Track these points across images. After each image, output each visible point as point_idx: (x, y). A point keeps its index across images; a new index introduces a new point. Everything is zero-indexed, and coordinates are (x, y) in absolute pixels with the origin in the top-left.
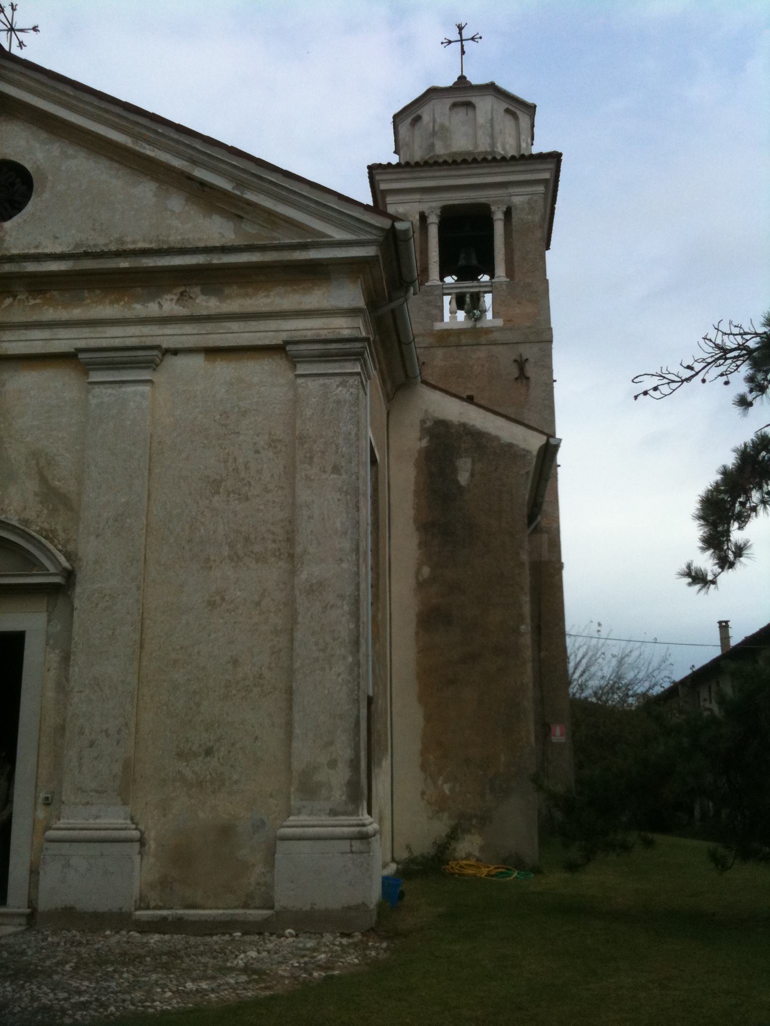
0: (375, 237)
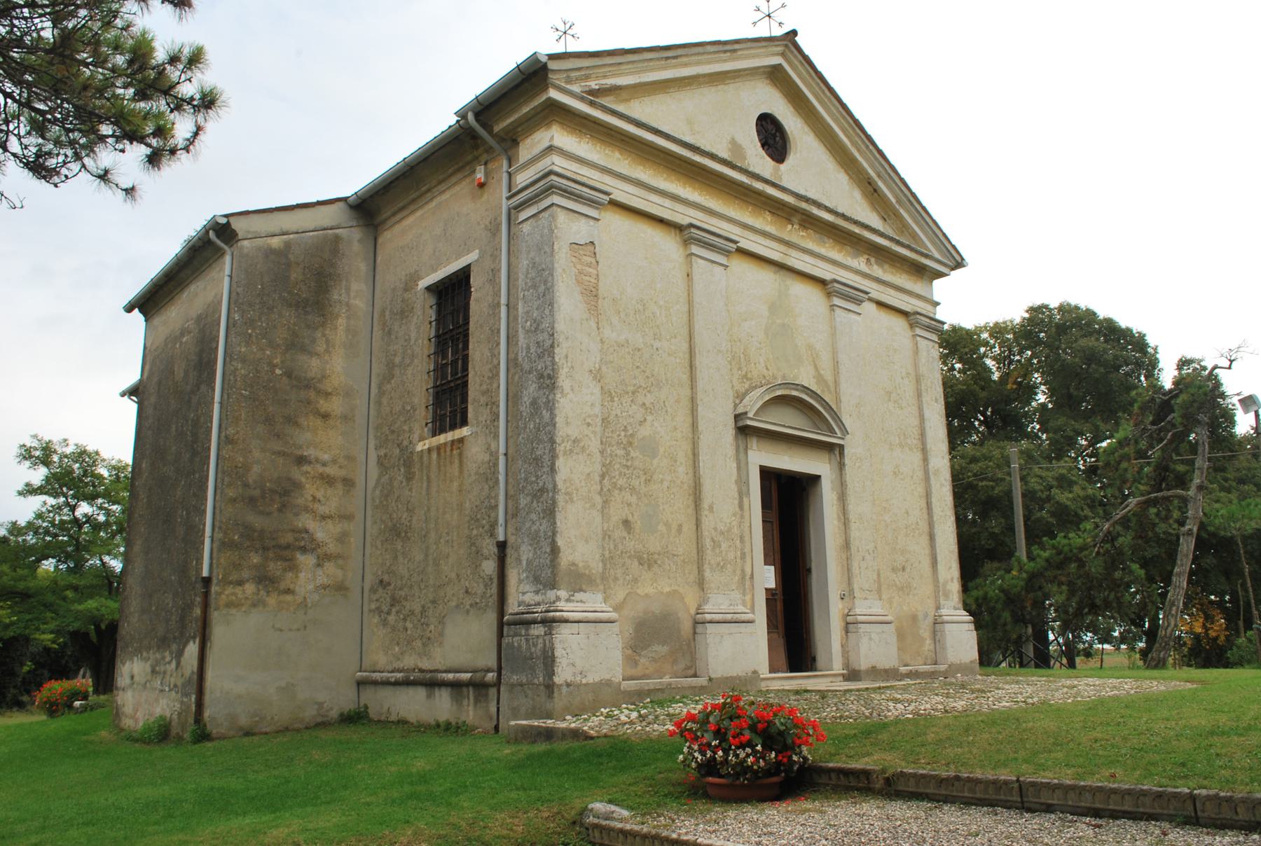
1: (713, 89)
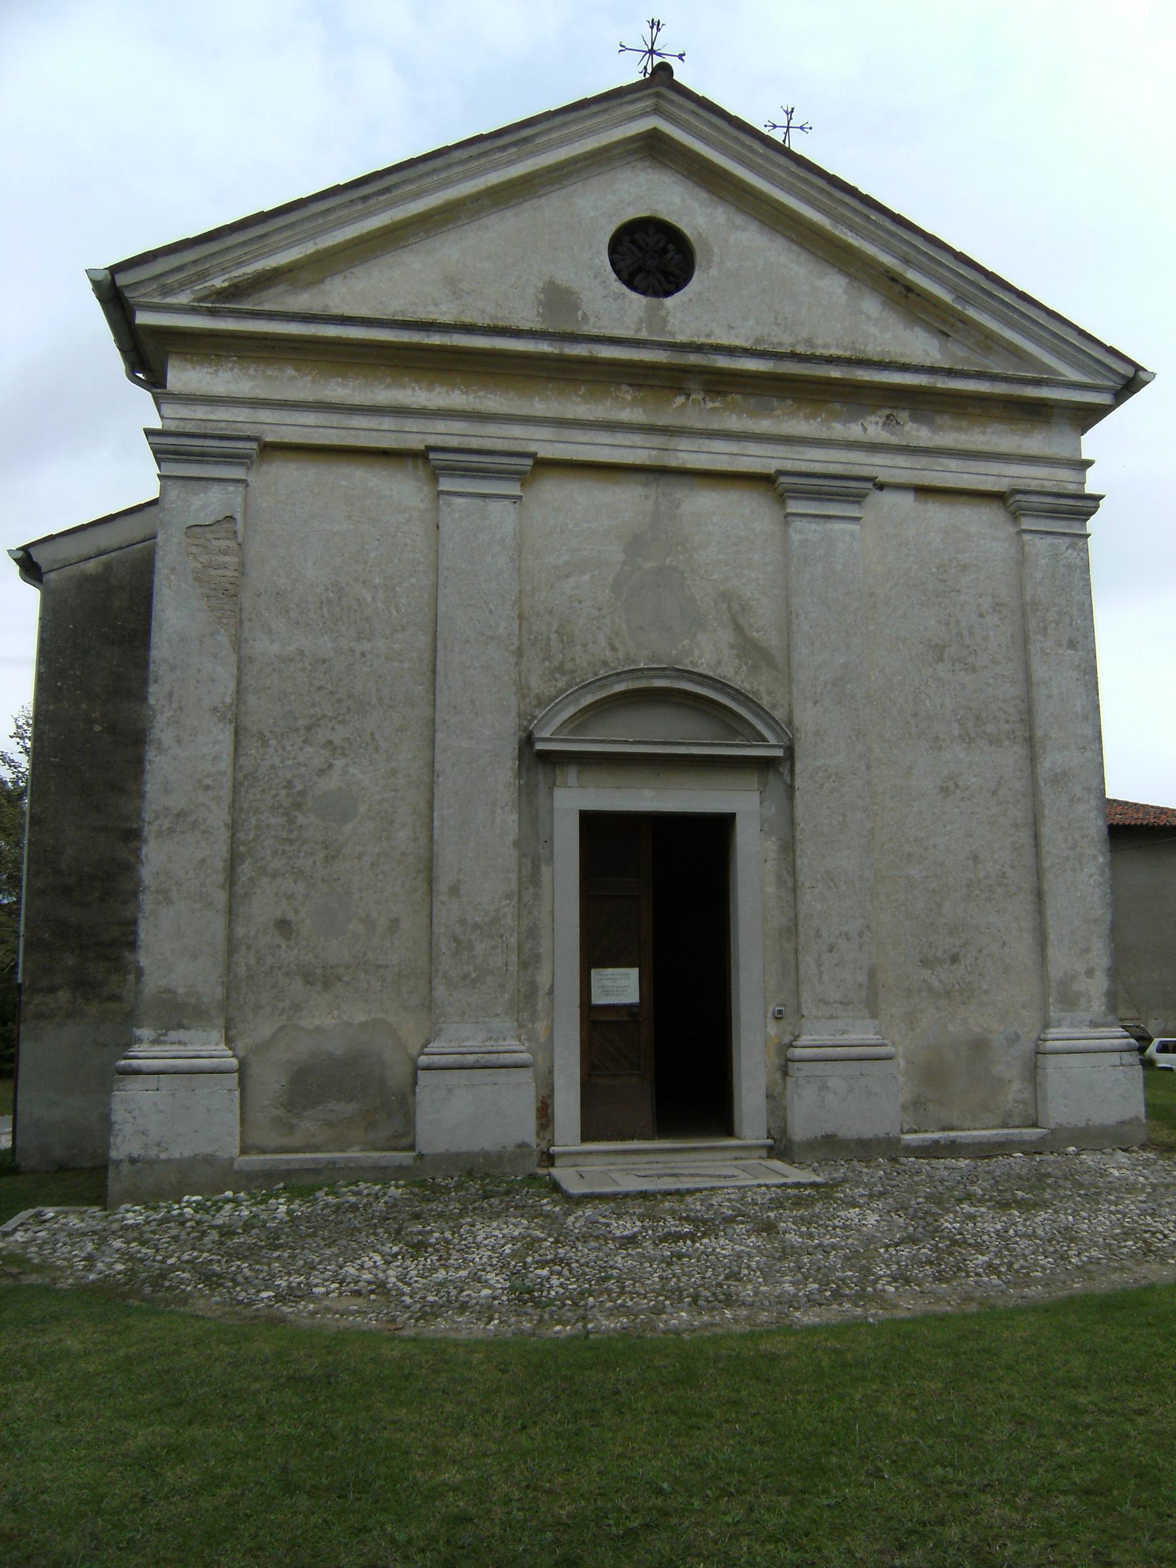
0: (1112, 384)
1: (510, 213)
